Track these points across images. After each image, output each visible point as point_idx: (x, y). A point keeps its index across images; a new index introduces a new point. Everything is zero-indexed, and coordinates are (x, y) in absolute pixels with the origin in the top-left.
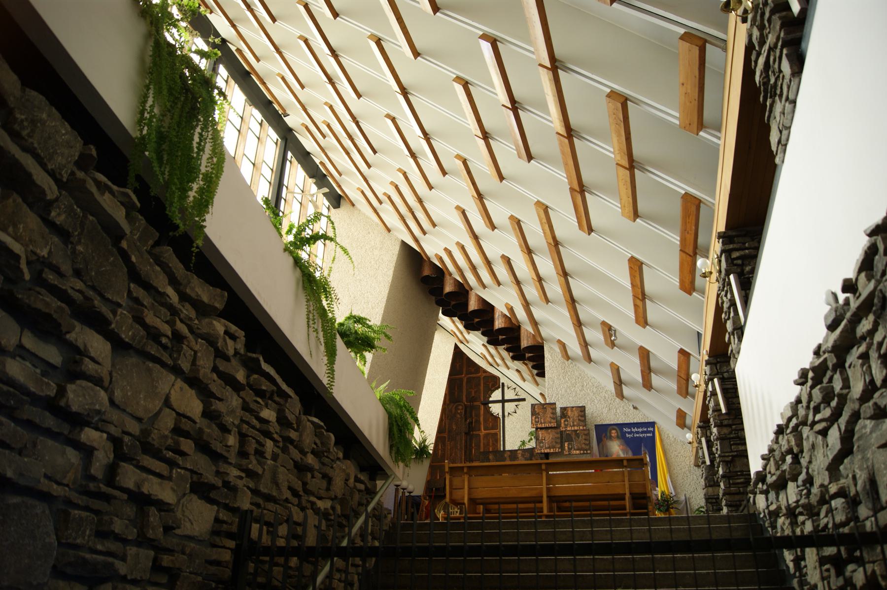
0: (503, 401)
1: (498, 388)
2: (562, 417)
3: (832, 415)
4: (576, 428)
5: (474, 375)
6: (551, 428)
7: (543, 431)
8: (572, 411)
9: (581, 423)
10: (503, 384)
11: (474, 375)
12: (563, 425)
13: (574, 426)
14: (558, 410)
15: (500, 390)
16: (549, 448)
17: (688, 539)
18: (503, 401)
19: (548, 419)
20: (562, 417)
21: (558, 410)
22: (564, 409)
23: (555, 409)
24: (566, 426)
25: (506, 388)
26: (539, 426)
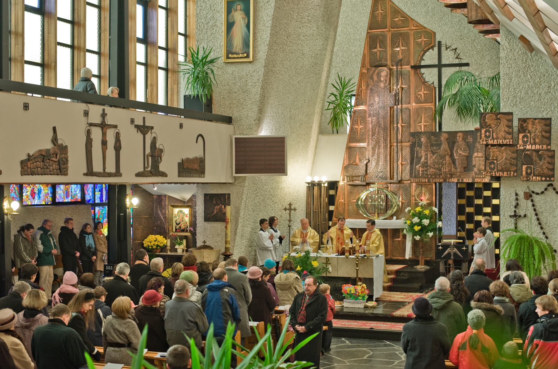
0: (440, 66)
1: (432, 48)
2: (519, 132)
3: (63, 314)
4: (538, 147)
5: (412, 96)
6: (506, 145)
7: (495, 149)
8: (533, 124)
9: (545, 140)
10: (439, 43)
11: (412, 96)
12: (521, 142)
13: (535, 144)
14: (516, 123)
15: (436, 49)
16: (502, 171)
17: (20, 81)
18: (440, 66)
19: (502, 134)
20: (519, 132)
21: (516, 123)
22: (523, 121)
23: (511, 121)
24: (525, 143)
25: (443, 48)
26: (490, 142)
